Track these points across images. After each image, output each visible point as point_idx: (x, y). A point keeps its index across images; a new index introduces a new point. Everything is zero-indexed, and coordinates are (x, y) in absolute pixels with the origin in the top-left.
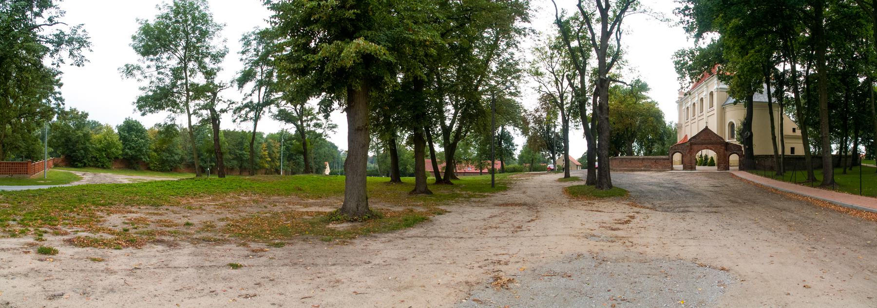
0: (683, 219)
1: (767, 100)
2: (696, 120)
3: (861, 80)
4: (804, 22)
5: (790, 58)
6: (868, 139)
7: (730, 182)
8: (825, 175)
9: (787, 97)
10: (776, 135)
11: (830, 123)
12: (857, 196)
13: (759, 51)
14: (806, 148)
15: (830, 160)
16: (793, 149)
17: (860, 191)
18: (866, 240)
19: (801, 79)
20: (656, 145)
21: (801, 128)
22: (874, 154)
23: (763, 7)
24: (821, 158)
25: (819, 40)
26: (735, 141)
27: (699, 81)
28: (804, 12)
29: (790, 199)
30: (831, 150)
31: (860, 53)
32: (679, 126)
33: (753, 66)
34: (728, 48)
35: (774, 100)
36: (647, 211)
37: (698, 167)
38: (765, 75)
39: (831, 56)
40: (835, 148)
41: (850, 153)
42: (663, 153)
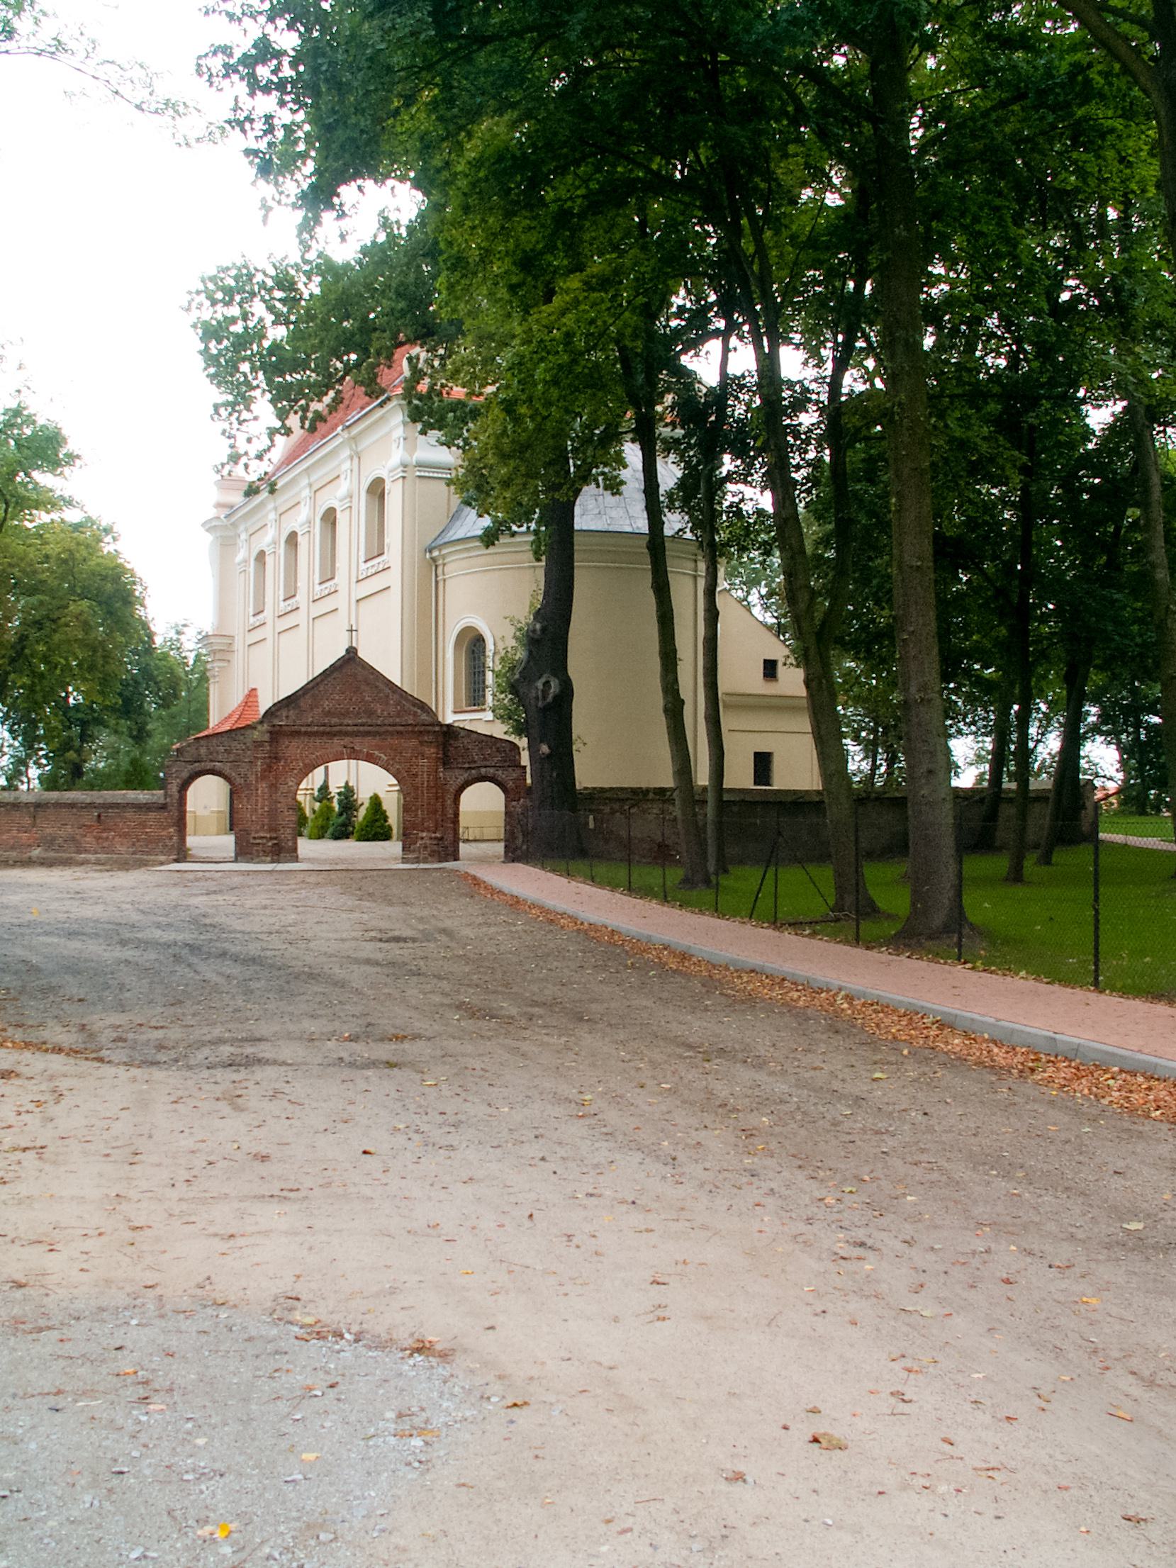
0: (234, 1100)
1: (642, 525)
2: (300, 618)
3: (1099, 417)
4: (822, 133)
5: (753, 318)
6: (1133, 713)
7: (460, 917)
8: (919, 884)
9: (736, 511)
10: (685, 692)
11: (944, 633)
12: (1079, 994)
13: (605, 283)
14: (831, 757)
15: (945, 817)
16: (763, 763)
17: (1092, 967)
18: (1120, 1214)
19: (807, 419)
20: (104, 738)
21: (804, 658)
22: (1161, 784)
23: (628, 58)
24: (900, 803)
25: (891, 222)
26: (485, 722)
27: (315, 424)
28: (819, 76)
29: (750, 1001)
30: (951, 767)
31: (1092, 280)
32: (218, 646)
33: (576, 356)
34: (458, 263)
35: (674, 522)
36: (57, 1062)
37: (305, 846)
38: (635, 402)
39: (949, 301)
40: (967, 758)
41: (1042, 782)
42: (136, 777)
